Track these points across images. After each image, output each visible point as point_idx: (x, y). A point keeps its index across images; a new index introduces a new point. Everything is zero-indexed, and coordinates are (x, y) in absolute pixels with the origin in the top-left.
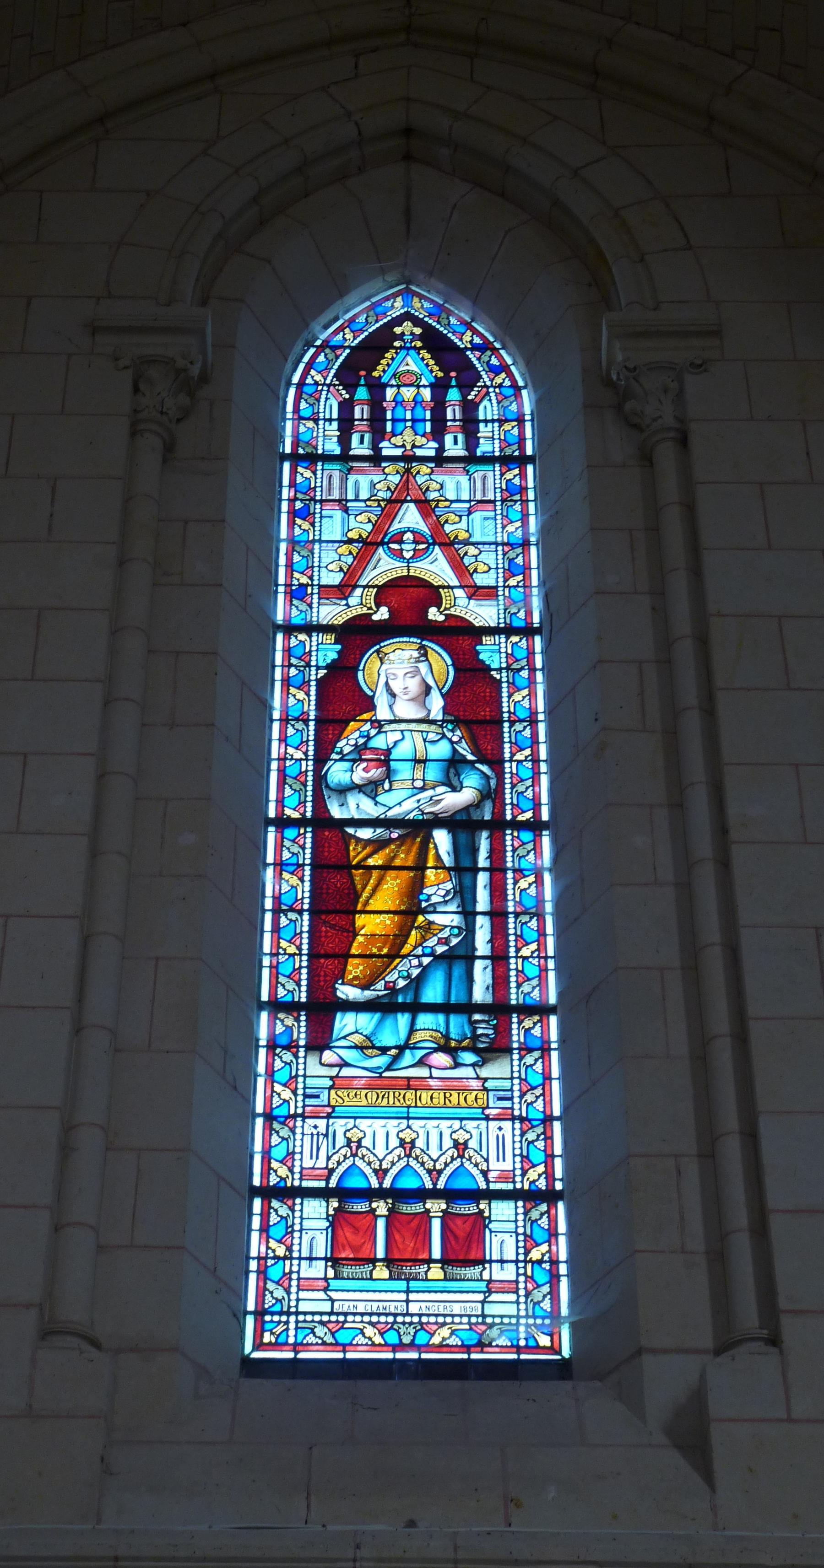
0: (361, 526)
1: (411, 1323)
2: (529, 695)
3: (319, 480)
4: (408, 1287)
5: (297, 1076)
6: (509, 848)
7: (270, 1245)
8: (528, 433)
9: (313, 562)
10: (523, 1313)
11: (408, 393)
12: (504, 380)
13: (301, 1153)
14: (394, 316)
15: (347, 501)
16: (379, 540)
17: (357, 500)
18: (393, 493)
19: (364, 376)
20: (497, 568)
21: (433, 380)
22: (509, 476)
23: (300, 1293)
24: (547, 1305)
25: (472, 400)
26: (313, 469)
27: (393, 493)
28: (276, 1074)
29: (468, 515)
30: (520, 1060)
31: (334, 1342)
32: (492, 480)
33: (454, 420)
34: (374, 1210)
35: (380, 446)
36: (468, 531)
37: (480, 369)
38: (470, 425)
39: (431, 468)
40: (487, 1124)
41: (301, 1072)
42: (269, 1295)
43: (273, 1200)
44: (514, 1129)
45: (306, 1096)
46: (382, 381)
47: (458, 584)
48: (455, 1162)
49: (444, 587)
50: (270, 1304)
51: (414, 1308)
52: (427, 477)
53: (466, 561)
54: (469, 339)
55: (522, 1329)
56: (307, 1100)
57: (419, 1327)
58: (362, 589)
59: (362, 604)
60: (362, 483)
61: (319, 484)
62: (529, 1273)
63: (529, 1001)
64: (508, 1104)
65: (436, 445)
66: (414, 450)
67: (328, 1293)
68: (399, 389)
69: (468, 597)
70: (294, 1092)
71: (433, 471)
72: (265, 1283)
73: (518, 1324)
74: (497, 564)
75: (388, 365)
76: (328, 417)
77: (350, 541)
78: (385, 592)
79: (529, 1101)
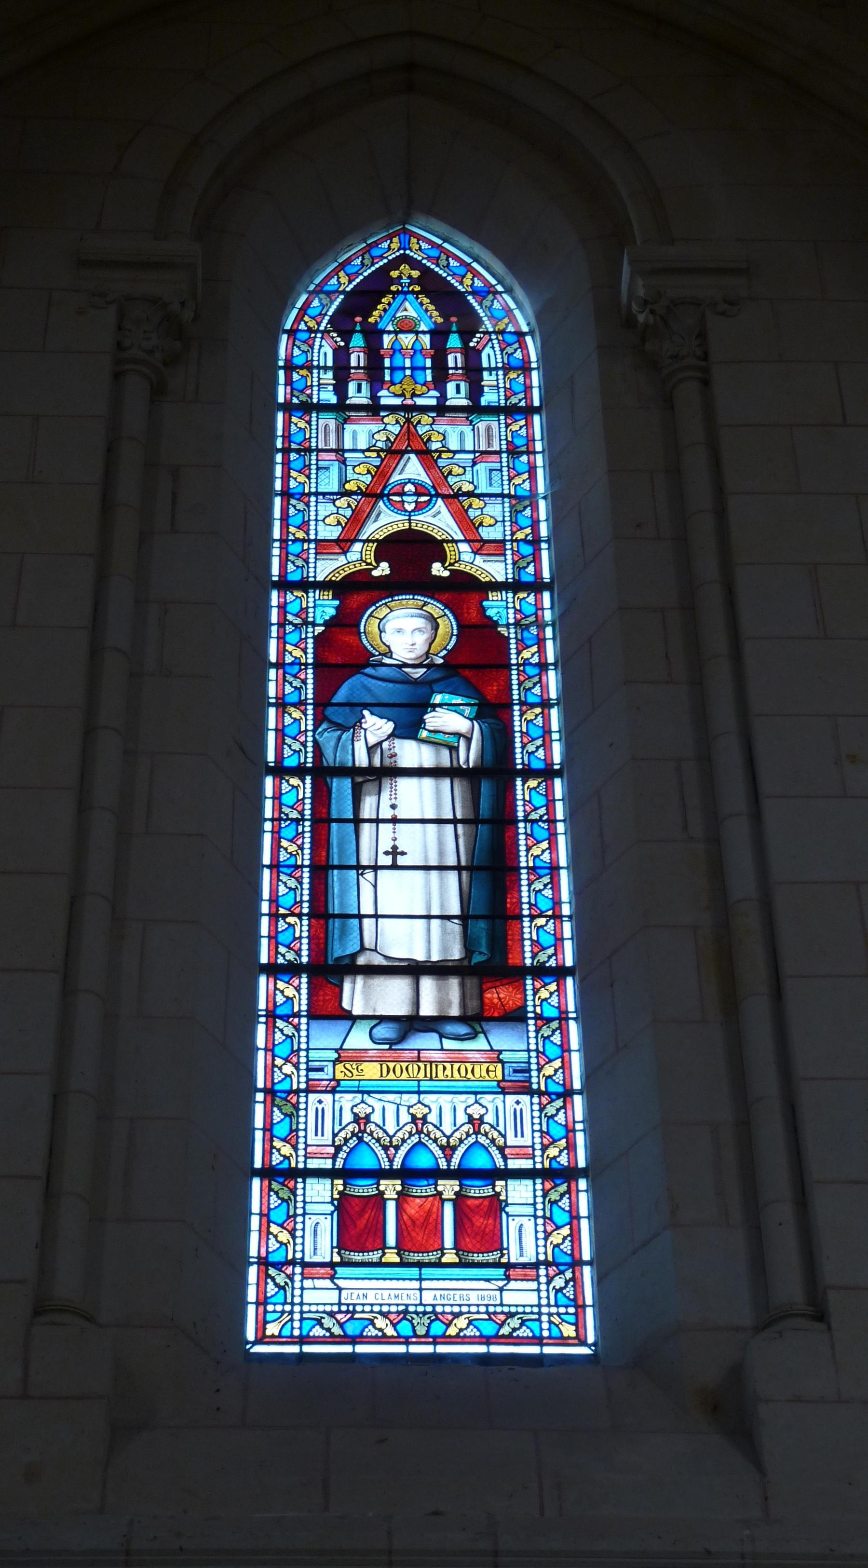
1: (425, 1313)
3: (314, 431)
4: (420, 1274)
6: (515, 682)
7: (275, 1144)
8: (535, 381)
9: (312, 381)
11: (407, 340)
13: (305, 1130)
14: (390, 258)
15: (344, 451)
17: (354, 451)
19: (360, 323)
21: (433, 326)
22: (514, 427)
23: (305, 1281)
25: (474, 347)
26: (307, 418)
28: (283, 830)
29: (472, 467)
32: (494, 431)
33: (456, 368)
35: (379, 395)
36: (472, 483)
37: (482, 314)
38: (473, 372)
39: (432, 417)
40: (501, 1101)
41: (303, 1046)
42: (277, 1153)
44: (532, 1104)
45: (309, 1070)
49: (448, 542)
50: (278, 1161)
51: (428, 1297)
52: (428, 428)
53: (472, 513)
54: (469, 282)
57: (434, 1317)
58: (361, 544)
59: (361, 560)
60: (361, 434)
61: (314, 435)
65: (438, 395)
67: (336, 1281)
68: (396, 336)
70: (296, 1066)
71: (434, 421)
72: (285, 646)
73: (540, 1314)
74: (504, 517)
75: (385, 310)
76: (322, 364)
77: (349, 494)
78: (386, 548)
79: (557, 1287)
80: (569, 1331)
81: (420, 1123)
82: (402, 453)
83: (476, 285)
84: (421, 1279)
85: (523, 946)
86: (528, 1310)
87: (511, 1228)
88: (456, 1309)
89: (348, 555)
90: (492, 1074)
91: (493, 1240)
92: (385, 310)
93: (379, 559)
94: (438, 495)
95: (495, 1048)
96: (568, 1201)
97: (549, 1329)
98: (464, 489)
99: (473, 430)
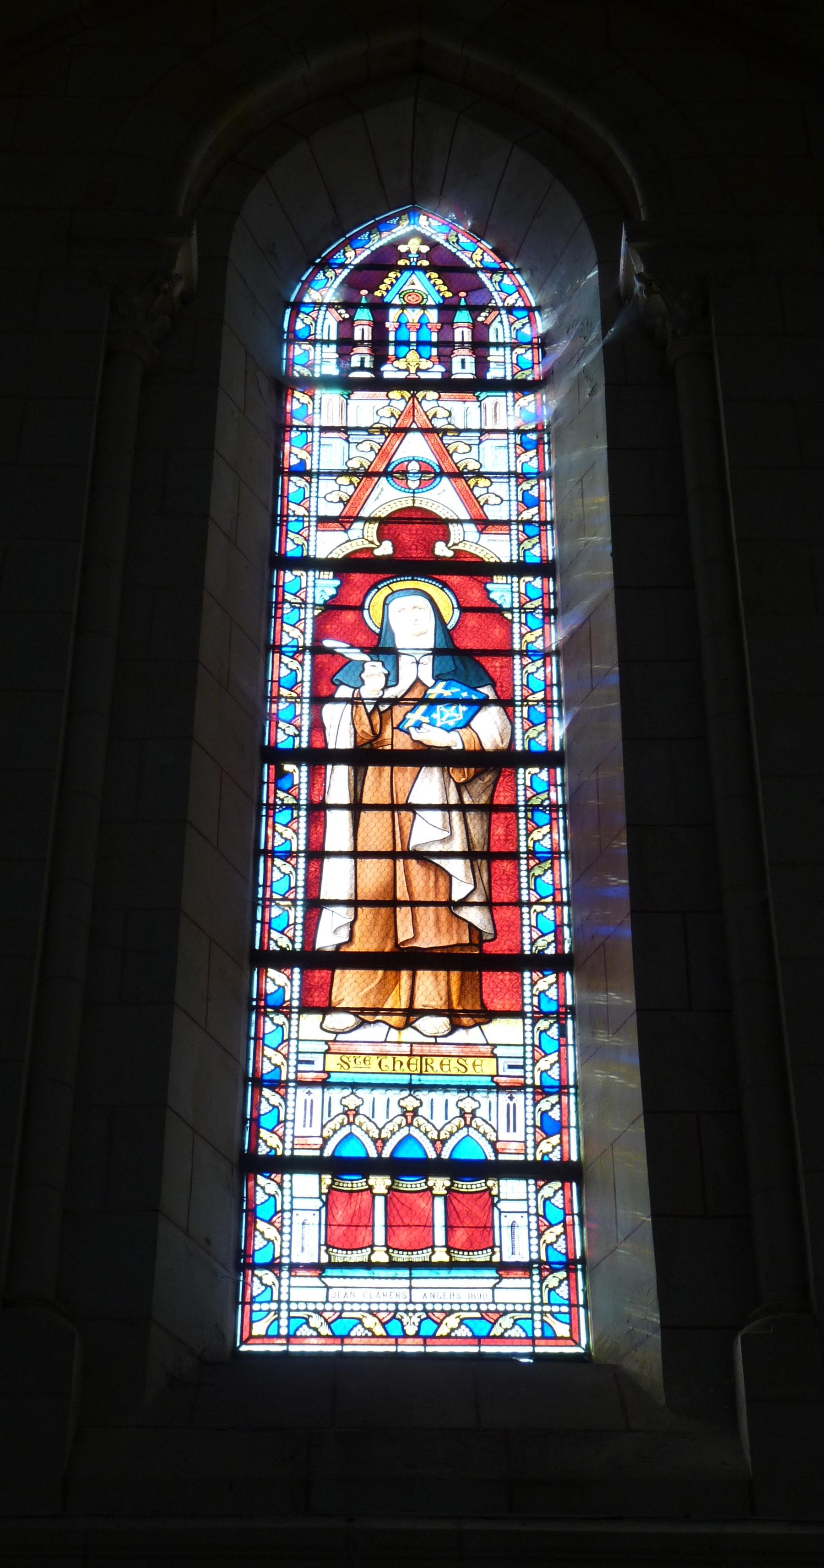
0: (362, 454)
1: (414, 1312)
2: (559, 1061)
5: (289, 1039)
10: (537, 1300)
11: (413, 315)
12: (516, 300)
16: (381, 470)
18: (397, 420)
19: (465, 297)
20: (510, 500)
24: (564, 1291)
27: (397, 420)
29: (479, 445)
30: (541, 1281)
31: (330, 1334)
34: (371, 1188)
35: (382, 369)
38: (480, 346)
41: (294, 1035)
43: (269, 970)
46: (385, 300)
47: (468, 518)
48: (460, 1131)
54: (479, 258)
55: (537, 1317)
56: (299, 1066)
62: (523, 621)
63: (535, 748)
64: (520, 1072)
65: (443, 370)
66: (419, 374)
69: (478, 531)
70: (286, 1057)
75: (392, 285)
78: (388, 525)
80: (563, 1330)
81: (468, 1117)
82: (406, 430)
83: (485, 260)
84: (410, 1278)
85: (522, 932)
86: (519, 1308)
87: (502, 1223)
88: (447, 1307)
89: (350, 532)
90: (446, 1068)
91: (483, 1233)
92: (392, 285)
93: (381, 537)
94: (441, 474)
95: (490, 1042)
96: (564, 1242)
97: (542, 1329)
98: (470, 468)
99: (480, 406)
